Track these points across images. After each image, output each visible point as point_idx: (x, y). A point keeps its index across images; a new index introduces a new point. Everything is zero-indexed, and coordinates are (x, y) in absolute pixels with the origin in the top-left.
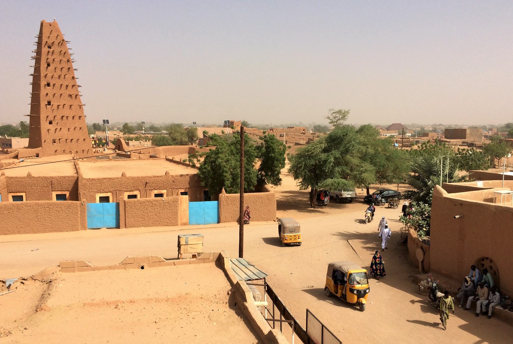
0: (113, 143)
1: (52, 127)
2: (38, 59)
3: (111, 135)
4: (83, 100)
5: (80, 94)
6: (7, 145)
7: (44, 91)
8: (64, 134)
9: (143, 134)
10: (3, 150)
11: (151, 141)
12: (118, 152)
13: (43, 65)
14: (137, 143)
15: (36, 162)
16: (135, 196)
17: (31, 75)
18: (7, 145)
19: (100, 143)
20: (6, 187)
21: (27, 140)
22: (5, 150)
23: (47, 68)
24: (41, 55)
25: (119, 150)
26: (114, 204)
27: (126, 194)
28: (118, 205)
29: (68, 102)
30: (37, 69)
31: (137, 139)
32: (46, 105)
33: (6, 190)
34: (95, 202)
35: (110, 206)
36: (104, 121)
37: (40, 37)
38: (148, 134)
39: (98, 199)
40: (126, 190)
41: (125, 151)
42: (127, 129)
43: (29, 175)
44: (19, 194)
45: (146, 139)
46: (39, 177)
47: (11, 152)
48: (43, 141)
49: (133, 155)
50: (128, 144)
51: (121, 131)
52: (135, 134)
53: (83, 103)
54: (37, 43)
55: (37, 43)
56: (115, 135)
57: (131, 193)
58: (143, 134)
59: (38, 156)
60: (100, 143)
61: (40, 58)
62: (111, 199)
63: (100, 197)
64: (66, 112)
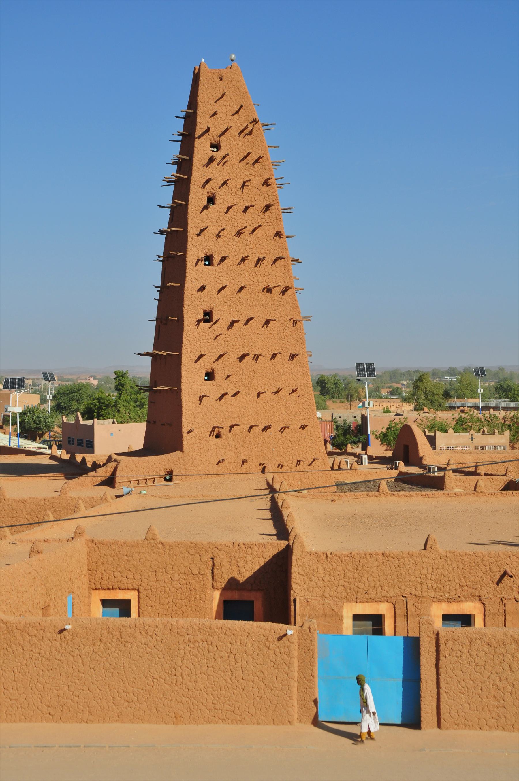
0: (384, 438)
1: (212, 389)
2: (181, 187)
3: (378, 413)
4: (305, 302)
5: (296, 284)
6: (80, 443)
7: (195, 275)
8: (244, 409)
9: (477, 408)
10: (73, 457)
11: (507, 433)
12: (403, 468)
13: (197, 197)
14: (462, 438)
15: (165, 497)
16: (466, 620)
17: (162, 232)
18: (80, 443)
19: (348, 437)
20: (85, 571)
21: (141, 427)
22: (79, 458)
23: (206, 207)
24: (189, 173)
25: (407, 463)
26: (400, 641)
27: (438, 610)
28: (412, 646)
29: (260, 307)
30: (179, 214)
31: (461, 426)
32: (199, 322)
33: (85, 580)
34: (339, 631)
35: (390, 649)
36: (360, 368)
37: (190, 119)
38: (496, 408)
39: (348, 623)
40: (437, 594)
41: (423, 467)
42: (423, 391)
43: (149, 537)
44: (121, 595)
45: (492, 427)
46: (178, 544)
47: (95, 466)
48: (185, 430)
49: (451, 478)
50: (432, 441)
51: (405, 400)
52: (452, 408)
53: (303, 314)
54: (182, 135)
55: (182, 135)
56: (387, 411)
57: (454, 609)
58: (477, 408)
59: (169, 477)
60: (348, 437)
61: (189, 180)
62: (388, 625)
63: (252, 602)
64: (255, 339)
